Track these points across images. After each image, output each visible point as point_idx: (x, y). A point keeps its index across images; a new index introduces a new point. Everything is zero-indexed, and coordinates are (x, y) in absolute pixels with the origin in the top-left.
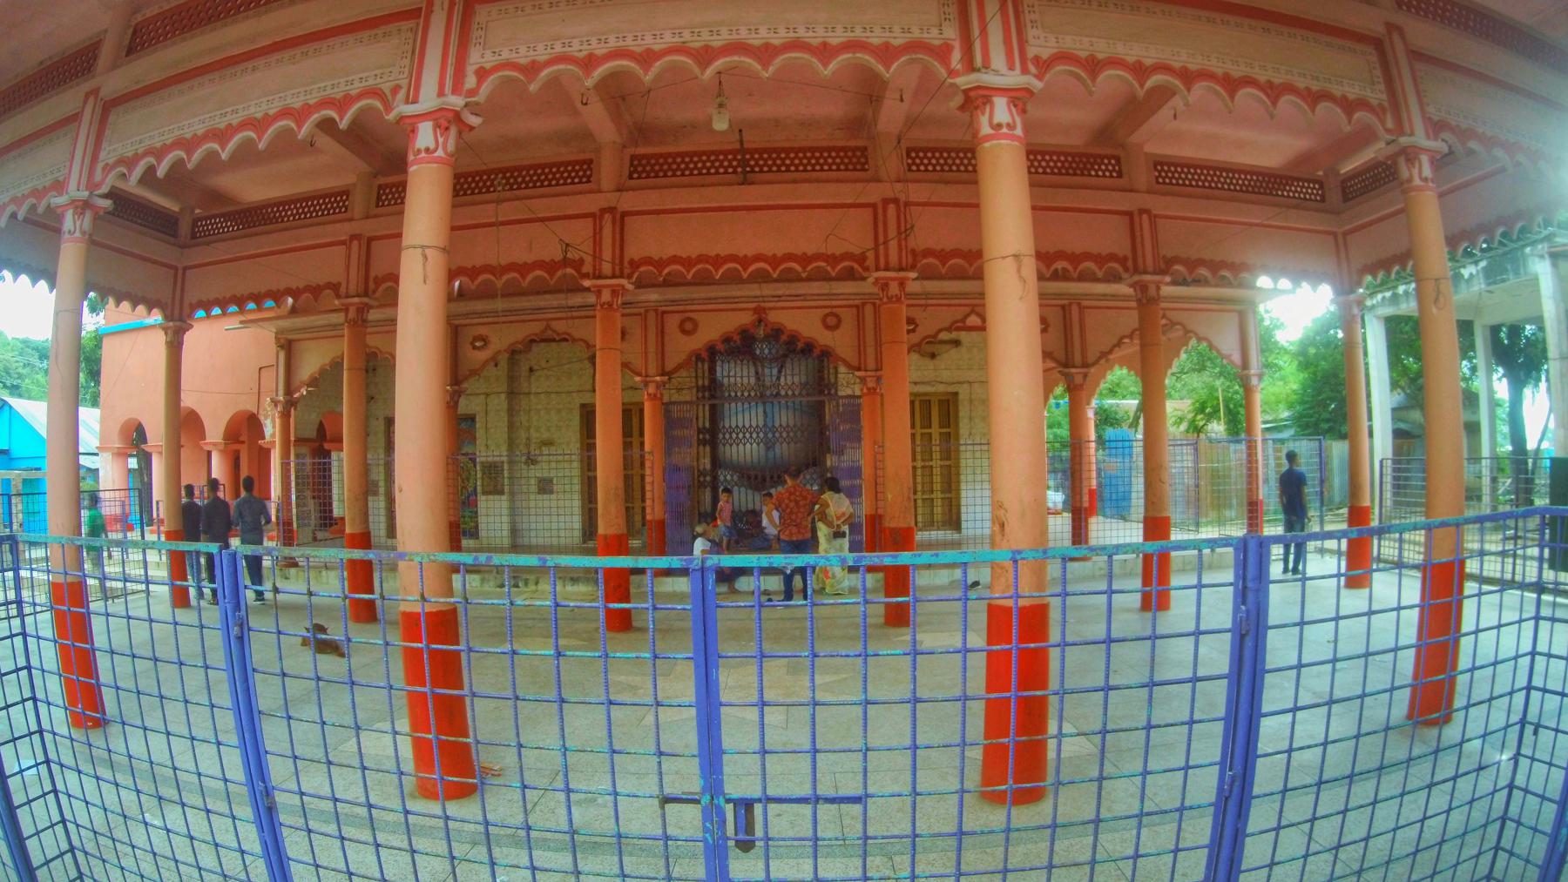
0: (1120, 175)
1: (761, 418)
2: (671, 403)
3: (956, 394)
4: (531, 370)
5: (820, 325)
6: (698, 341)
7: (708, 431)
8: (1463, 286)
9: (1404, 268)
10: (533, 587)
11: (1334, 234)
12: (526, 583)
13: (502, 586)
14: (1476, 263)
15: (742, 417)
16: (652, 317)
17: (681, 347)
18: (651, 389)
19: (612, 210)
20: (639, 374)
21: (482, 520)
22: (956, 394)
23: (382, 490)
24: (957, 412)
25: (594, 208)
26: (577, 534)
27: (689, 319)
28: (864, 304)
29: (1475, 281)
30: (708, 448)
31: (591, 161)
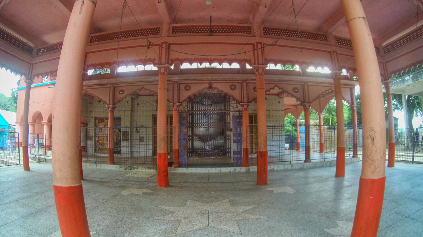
0: (327, 41)
1: (207, 120)
4: (138, 104)
5: (229, 89)
6: (190, 93)
7: (191, 124)
8: (406, 82)
9: (395, 75)
10: (136, 170)
11: (382, 63)
12: (134, 169)
13: (126, 169)
14: (409, 76)
15: (200, 119)
16: (176, 84)
17: (185, 95)
18: (175, 107)
19: (165, 42)
20: (171, 103)
21: (122, 150)
25: (160, 42)
26: (151, 153)
27: (188, 86)
28: (243, 82)
29: (409, 81)
30: (191, 129)
31: (159, 28)
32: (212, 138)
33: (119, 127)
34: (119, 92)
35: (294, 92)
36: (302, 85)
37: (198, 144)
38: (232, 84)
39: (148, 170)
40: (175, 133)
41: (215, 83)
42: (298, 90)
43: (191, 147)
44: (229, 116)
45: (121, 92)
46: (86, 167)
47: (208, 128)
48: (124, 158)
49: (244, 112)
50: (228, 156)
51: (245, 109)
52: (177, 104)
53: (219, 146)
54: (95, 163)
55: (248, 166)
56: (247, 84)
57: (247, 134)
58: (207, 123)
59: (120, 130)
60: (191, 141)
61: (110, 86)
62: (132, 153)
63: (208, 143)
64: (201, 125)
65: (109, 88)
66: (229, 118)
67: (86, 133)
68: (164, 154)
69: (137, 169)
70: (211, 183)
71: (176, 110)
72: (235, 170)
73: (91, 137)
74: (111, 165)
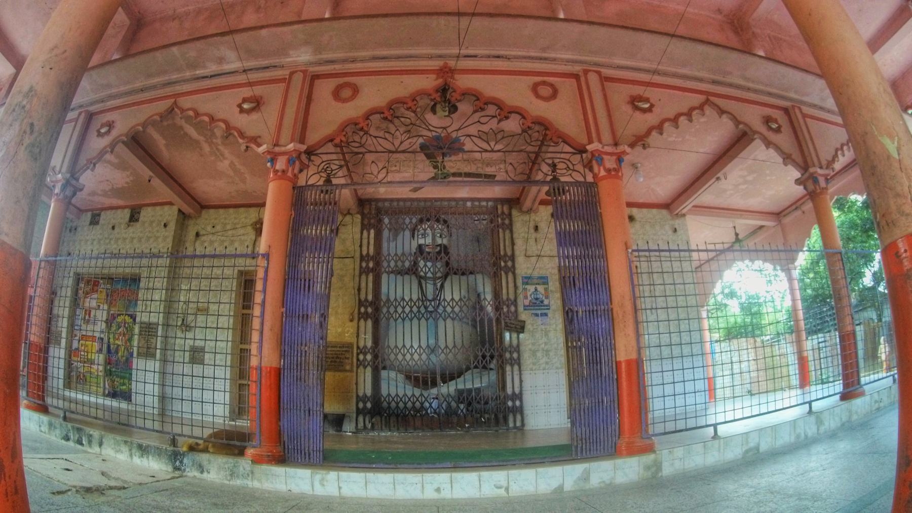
6: (352, 110)
7: (371, 304)
23: (63, 341)
27: (347, 85)
28: (586, 72)
30: (370, 323)
39: (137, 460)
43: (369, 392)
49: (604, 187)
50: (511, 425)
51: (608, 171)
55: (649, 449)
59: (134, 318)
60: (369, 369)
66: (511, 285)
71: (282, 175)
72: (586, 477)
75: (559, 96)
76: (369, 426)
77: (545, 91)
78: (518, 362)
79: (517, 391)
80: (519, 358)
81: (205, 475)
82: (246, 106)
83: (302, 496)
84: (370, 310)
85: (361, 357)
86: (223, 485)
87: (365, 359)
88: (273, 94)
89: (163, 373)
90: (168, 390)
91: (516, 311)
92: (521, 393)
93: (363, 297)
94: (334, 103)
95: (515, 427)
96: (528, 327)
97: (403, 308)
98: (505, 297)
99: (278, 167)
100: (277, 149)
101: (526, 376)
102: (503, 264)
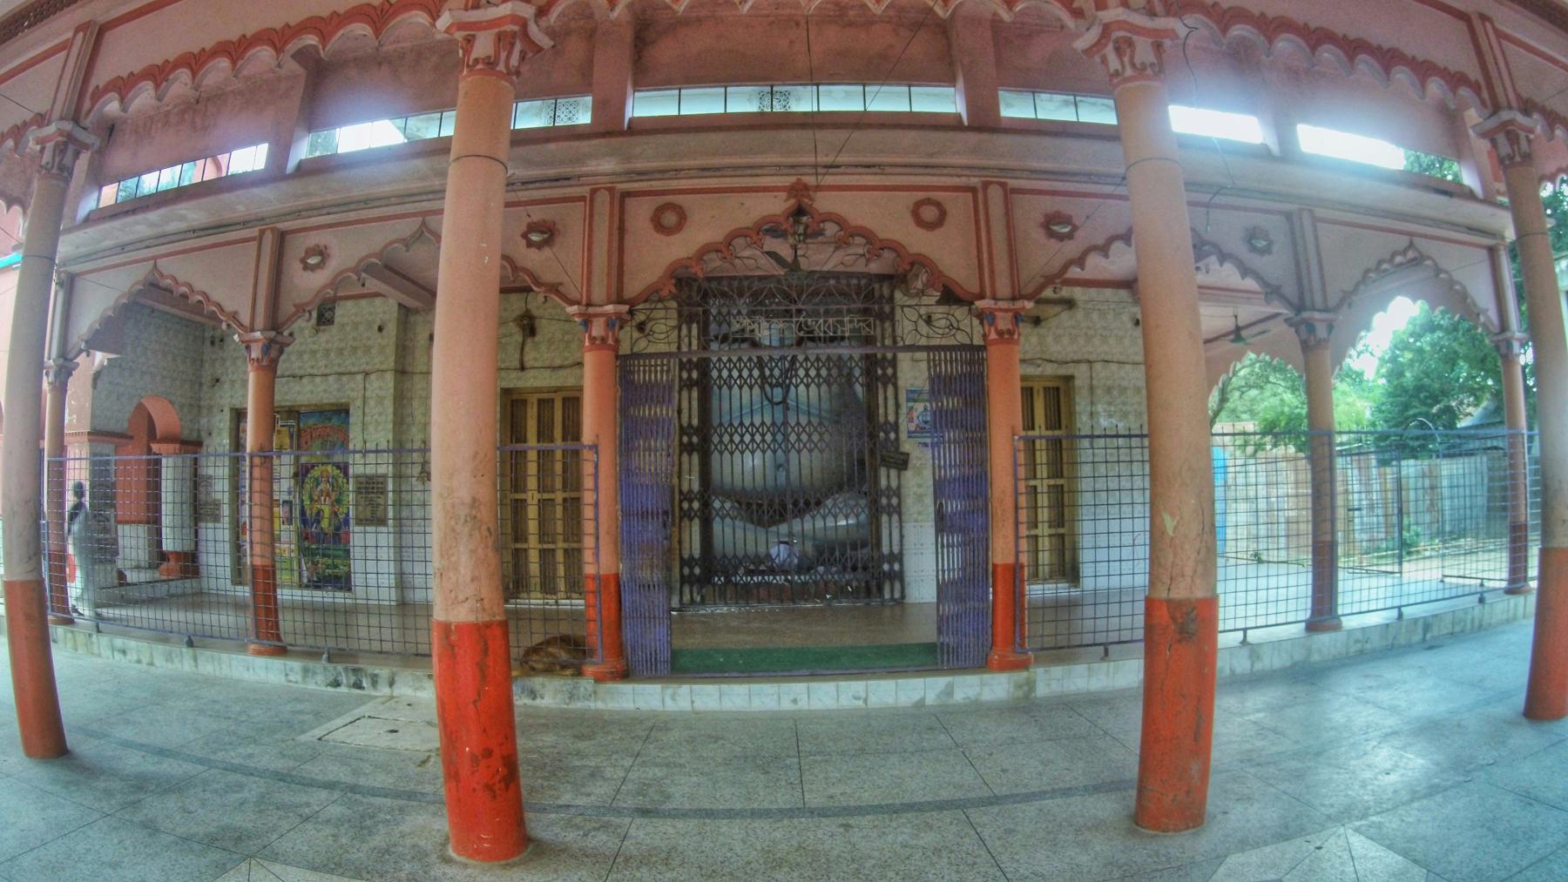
2: (635, 356)
3: (1069, 379)
6: (679, 248)
7: (697, 431)
10: (384, 690)
12: (374, 681)
13: (337, 684)
16: (603, 198)
17: (655, 257)
18: (598, 329)
21: (357, 566)
22: (1069, 379)
24: (1071, 405)
28: (986, 185)
30: (696, 458)
32: (807, 503)
33: (338, 458)
34: (303, 261)
35: (1254, 249)
36: (1288, 216)
37: (733, 535)
38: (921, 195)
40: (596, 476)
41: (818, 188)
42: (1270, 244)
43: (697, 553)
44: (890, 389)
45: (312, 261)
46: (151, 664)
47: (787, 452)
48: (368, 611)
49: (995, 354)
50: (887, 596)
51: (1000, 333)
52: (610, 308)
53: (843, 545)
54: (190, 644)
55: (1023, 665)
56: (1009, 193)
57: (1016, 479)
58: (780, 428)
59: (344, 468)
60: (696, 522)
61: (262, 232)
62: (402, 583)
63: (783, 528)
64: (747, 438)
65: (254, 244)
66: (891, 402)
67: (196, 486)
68: (480, 631)
69: (392, 684)
70: (823, 813)
71: (600, 343)
72: (949, 691)
73: (217, 504)
74: (261, 661)
75: (949, 219)
76: (698, 599)
77: (929, 213)
78: (898, 510)
79: (896, 550)
80: (899, 505)
81: (538, 701)
82: (535, 238)
83: (654, 715)
84: (695, 439)
85: (685, 505)
86: (563, 711)
87: (691, 508)
88: (572, 219)
89: (399, 548)
90: (407, 567)
91: (897, 439)
92: (901, 553)
93: (685, 422)
94: (656, 235)
95: (892, 598)
96: (913, 461)
97: (742, 436)
98: (882, 419)
99: (594, 333)
100: (591, 310)
101: (909, 528)
102: (880, 372)
